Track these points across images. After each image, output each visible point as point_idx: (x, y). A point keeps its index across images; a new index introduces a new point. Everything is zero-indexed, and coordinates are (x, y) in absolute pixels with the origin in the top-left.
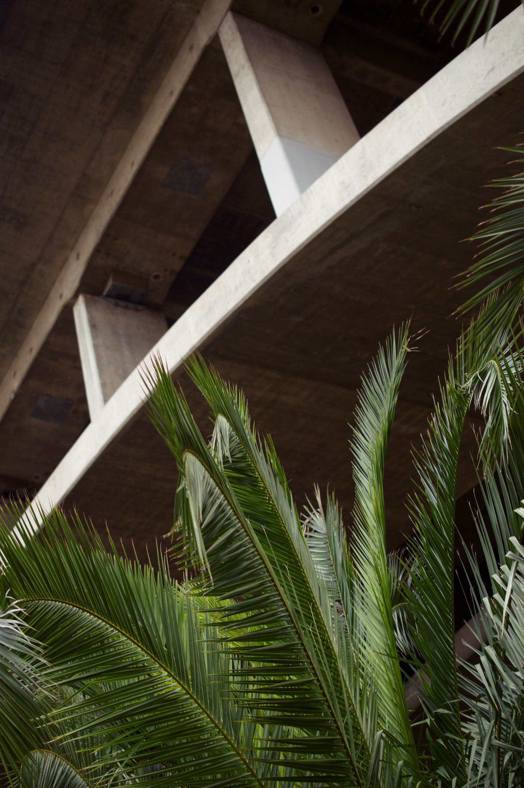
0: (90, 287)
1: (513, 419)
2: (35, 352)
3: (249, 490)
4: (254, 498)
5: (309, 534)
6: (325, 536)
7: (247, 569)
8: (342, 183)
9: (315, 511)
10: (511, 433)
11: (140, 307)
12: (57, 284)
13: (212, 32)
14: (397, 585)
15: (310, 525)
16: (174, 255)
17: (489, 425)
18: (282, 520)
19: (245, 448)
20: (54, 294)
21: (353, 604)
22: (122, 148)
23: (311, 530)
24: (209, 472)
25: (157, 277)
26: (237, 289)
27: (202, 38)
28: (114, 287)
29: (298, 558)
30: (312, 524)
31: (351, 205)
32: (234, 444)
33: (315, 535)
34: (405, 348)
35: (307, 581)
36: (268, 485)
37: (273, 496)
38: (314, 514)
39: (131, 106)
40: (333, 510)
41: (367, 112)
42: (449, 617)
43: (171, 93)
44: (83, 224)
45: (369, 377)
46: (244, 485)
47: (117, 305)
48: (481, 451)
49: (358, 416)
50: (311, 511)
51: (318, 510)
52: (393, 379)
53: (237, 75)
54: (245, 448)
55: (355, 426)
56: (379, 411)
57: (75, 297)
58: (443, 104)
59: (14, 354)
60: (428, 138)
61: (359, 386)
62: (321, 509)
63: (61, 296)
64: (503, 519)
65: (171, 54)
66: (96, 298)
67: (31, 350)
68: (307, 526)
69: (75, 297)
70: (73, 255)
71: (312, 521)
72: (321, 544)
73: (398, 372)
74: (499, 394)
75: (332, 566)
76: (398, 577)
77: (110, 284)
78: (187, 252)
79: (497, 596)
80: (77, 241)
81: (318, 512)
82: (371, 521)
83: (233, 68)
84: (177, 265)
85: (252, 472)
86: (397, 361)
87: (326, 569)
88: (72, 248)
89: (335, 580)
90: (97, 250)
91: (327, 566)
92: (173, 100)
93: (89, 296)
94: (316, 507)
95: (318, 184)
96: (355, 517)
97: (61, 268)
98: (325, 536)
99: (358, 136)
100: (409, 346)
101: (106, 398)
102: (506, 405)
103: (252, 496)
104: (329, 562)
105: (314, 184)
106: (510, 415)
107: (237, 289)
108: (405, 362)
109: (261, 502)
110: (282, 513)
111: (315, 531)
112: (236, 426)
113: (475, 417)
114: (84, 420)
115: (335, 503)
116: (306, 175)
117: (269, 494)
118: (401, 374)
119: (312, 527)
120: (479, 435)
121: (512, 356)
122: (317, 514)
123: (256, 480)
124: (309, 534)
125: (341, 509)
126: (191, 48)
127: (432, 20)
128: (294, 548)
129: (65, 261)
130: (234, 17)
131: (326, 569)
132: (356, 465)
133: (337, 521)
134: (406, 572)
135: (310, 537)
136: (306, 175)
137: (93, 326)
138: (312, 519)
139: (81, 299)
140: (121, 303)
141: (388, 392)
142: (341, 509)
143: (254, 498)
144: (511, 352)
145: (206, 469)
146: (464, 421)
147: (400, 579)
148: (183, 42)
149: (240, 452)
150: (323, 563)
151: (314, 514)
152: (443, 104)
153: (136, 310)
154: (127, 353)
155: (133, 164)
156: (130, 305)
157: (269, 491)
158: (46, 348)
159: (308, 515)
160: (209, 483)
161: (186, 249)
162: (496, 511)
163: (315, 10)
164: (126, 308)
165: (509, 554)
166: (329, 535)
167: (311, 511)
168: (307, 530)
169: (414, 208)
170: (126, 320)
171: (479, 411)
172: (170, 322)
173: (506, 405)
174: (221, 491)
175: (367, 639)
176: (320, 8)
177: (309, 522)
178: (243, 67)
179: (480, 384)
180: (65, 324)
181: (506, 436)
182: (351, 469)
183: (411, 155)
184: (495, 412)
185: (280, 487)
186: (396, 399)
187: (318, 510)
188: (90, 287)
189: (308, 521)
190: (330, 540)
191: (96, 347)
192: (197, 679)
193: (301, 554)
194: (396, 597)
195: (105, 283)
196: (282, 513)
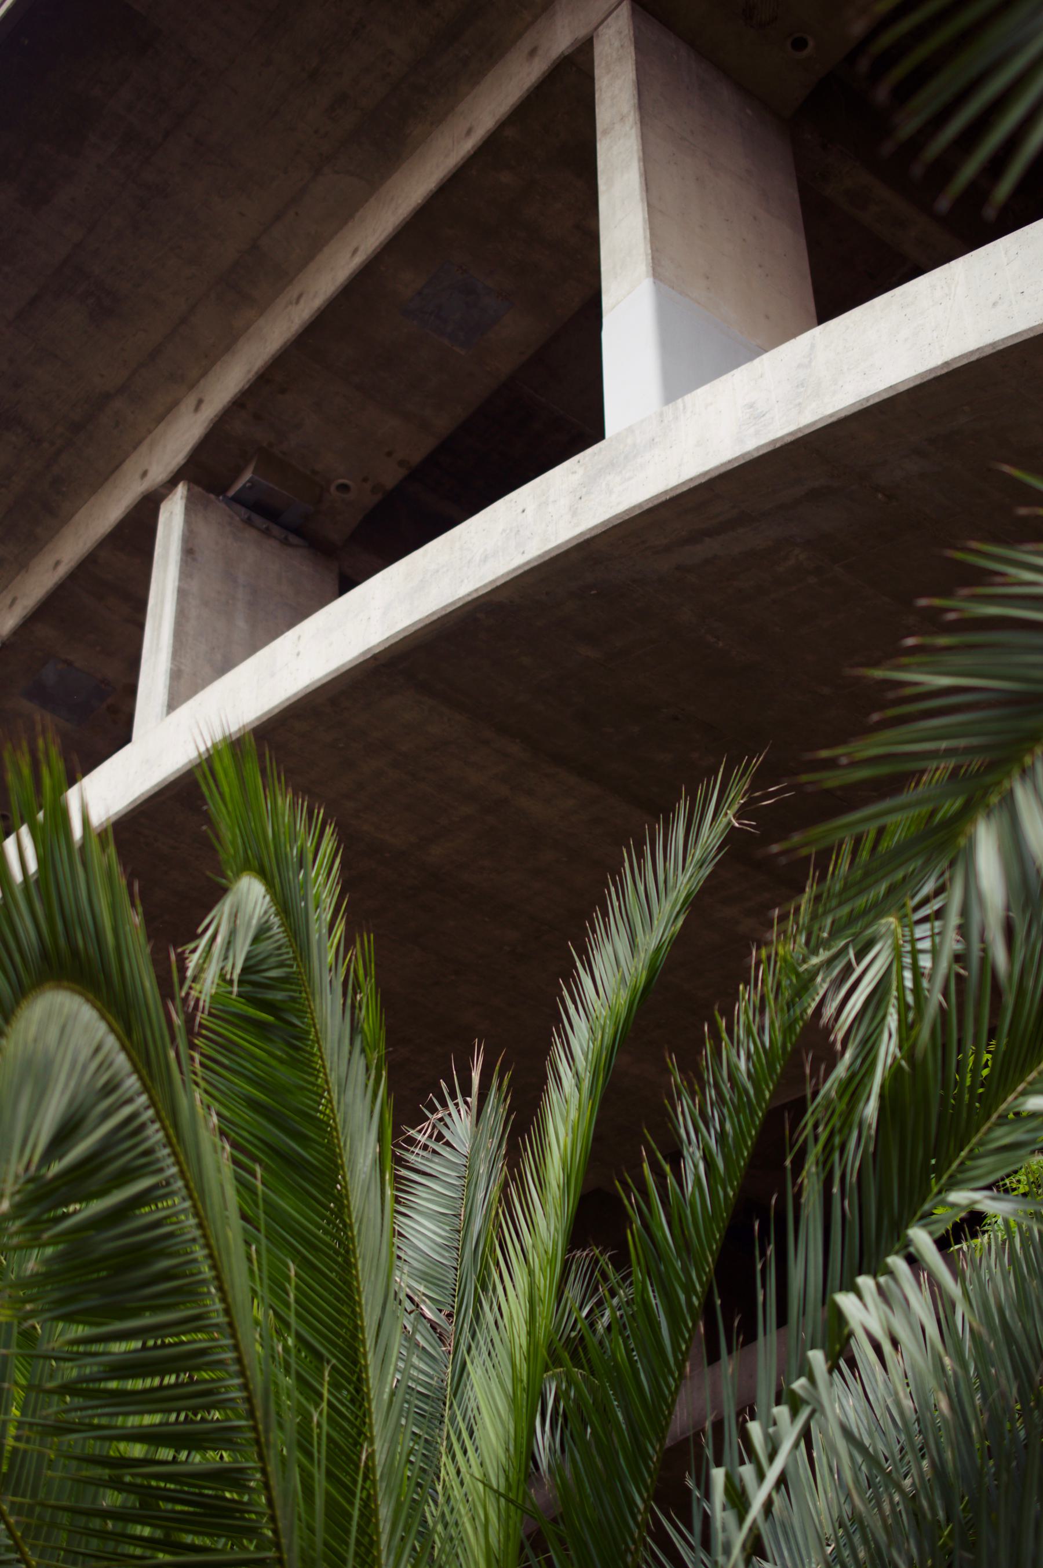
0: (204, 473)
1: (895, 1074)
2: (63, 570)
3: (279, 1053)
4: (285, 1075)
5: (432, 1145)
6: (464, 1161)
7: (167, 1275)
8: (751, 406)
9: (460, 1100)
10: (881, 1109)
11: (293, 539)
12: (143, 448)
13: (582, 32)
14: (573, 1329)
15: (440, 1126)
16: (389, 454)
17: (841, 1070)
18: (338, 1138)
19: (295, 959)
20: (131, 467)
21: (473, 1336)
22: (344, 213)
23: (440, 1137)
24: (119, 1038)
25: (344, 488)
26: (485, 559)
27: (560, 40)
28: (252, 484)
29: (352, 1232)
30: (446, 1125)
31: (756, 455)
32: (266, 946)
33: (445, 1152)
34: (729, 817)
35: (358, 1289)
36: (329, 1051)
37: (333, 1078)
38: (457, 1105)
39: (385, 138)
40: (496, 1109)
41: (845, 275)
42: (651, 1451)
43: (469, 132)
44: (226, 343)
45: (641, 855)
46: (271, 1040)
47: (248, 522)
48: (809, 1119)
49: (594, 931)
50: (454, 1097)
51: (468, 1099)
52: (685, 882)
53: (605, 132)
54: (295, 959)
55: (583, 952)
56: (640, 938)
57: (172, 483)
58: (995, 304)
59: (22, 564)
60: (946, 364)
61: (616, 871)
62: (473, 1100)
63: (144, 474)
64: (816, 1291)
65: (491, 53)
66: (212, 496)
67: (57, 563)
68: (434, 1127)
69: (172, 483)
70: (191, 400)
71: (447, 1120)
72: (452, 1176)
73: (701, 867)
74: (884, 1004)
75: (459, 1232)
76: (581, 1308)
77: (247, 476)
78: (416, 457)
79: (747, 1471)
80: (204, 374)
81: (466, 1103)
82: (555, 1172)
83: (604, 115)
84: (391, 476)
85: (298, 1017)
86: (710, 835)
87: (443, 1233)
88: (192, 386)
89: (455, 1265)
90: (238, 404)
91: (448, 1228)
92: (468, 145)
93: (197, 489)
94: (466, 1092)
95: (702, 393)
96: (525, 1150)
97: (160, 419)
98: (464, 1161)
99: (815, 320)
100: (738, 816)
101: (172, 706)
102: (890, 1035)
103: (283, 1068)
104: (456, 1221)
105: (695, 394)
106: (891, 1066)
107: (485, 559)
108: (720, 849)
109: (302, 1088)
110: (345, 1122)
111: (448, 1144)
112: (286, 904)
113: (813, 1043)
114: (120, 735)
115: (505, 1100)
116: (686, 370)
117: (325, 1074)
118: (707, 871)
119: (445, 1132)
120: (817, 1084)
121: (932, 929)
122: (463, 1108)
123: (302, 1036)
124: (432, 1145)
125: (513, 1117)
126: (533, 52)
127: (882, 94)
128: (348, 1207)
129: (173, 406)
130: (634, 13)
131: (443, 1233)
132: (560, 1036)
133: (496, 1141)
134: (600, 1303)
135: (434, 1152)
136: (686, 370)
137: (189, 552)
138: (450, 1115)
139: (181, 490)
140: (258, 520)
141: (673, 896)
142: (513, 1117)
143: (285, 1075)
144: (932, 917)
145: (112, 1030)
146: (802, 1029)
147: (584, 1314)
148: (519, 36)
149: (281, 965)
150: (442, 1218)
151: (457, 1105)
152: (995, 304)
153: (285, 542)
154: (241, 623)
155: (355, 251)
156: (276, 530)
157: (328, 1065)
158: (87, 567)
159: (445, 1105)
160: (111, 1065)
161: (417, 449)
162: (805, 1266)
163: (799, 44)
164: (266, 533)
165: (799, 1385)
166: (471, 1159)
167: (454, 1097)
168: (430, 1137)
169: (880, 496)
170: (259, 557)
171: (829, 1030)
172: (346, 584)
173: (890, 1035)
174: (144, 1084)
175: (475, 1434)
176: (811, 43)
177: (441, 1119)
178: (622, 119)
179: (848, 969)
180: (137, 532)
181: (871, 1110)
182: (547, 1046)
183: (902, 389)
184: (865, 1042)
185: (359, 1063)
186: (680, 923)
187: (468, 1099)
188: (204, 473)
189: (440, 1116)
190: (471, 1174)
191: (182, 594)
192: (22, 1466)
193: (361, 1223)
194: (564, 1349)
195: (238, 472)
196: (345, 1122)
